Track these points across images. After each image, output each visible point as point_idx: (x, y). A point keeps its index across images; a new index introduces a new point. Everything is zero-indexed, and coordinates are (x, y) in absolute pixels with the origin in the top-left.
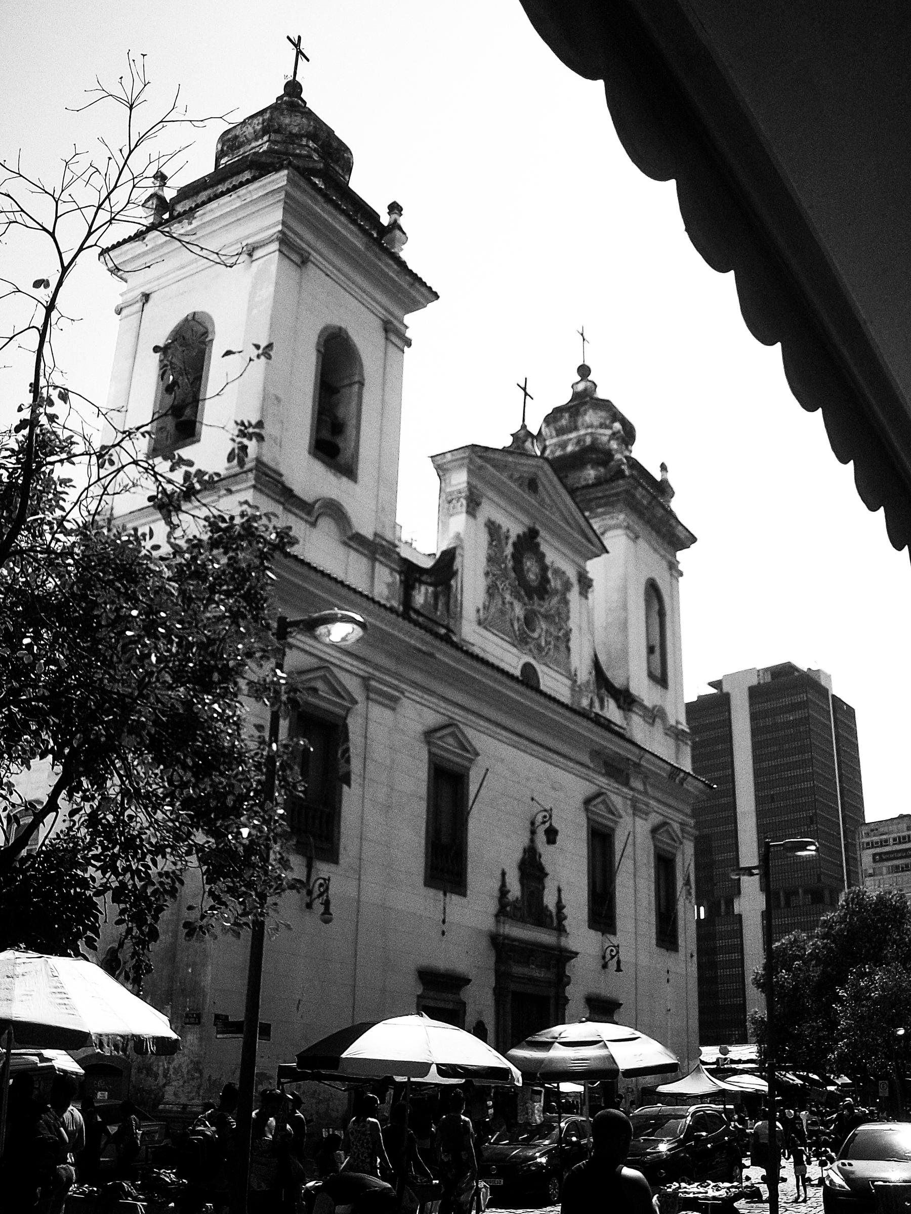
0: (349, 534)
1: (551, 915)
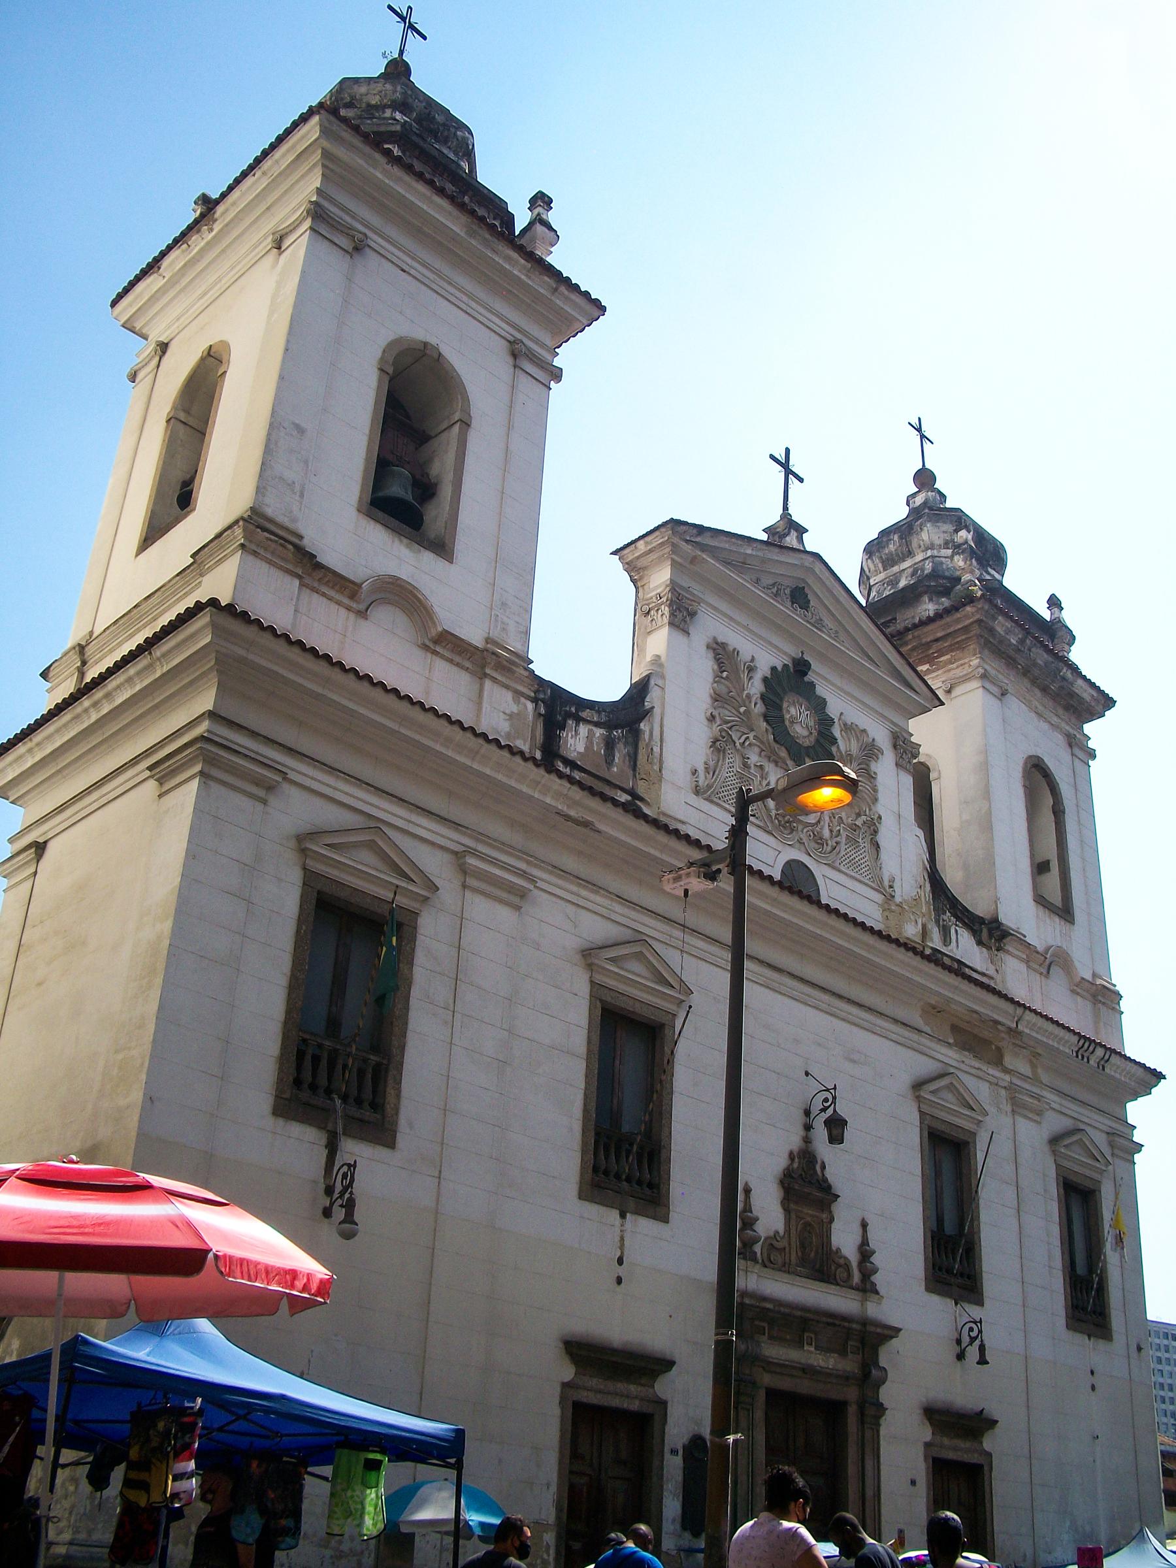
0: (433, 633)
1: (847, 1266)
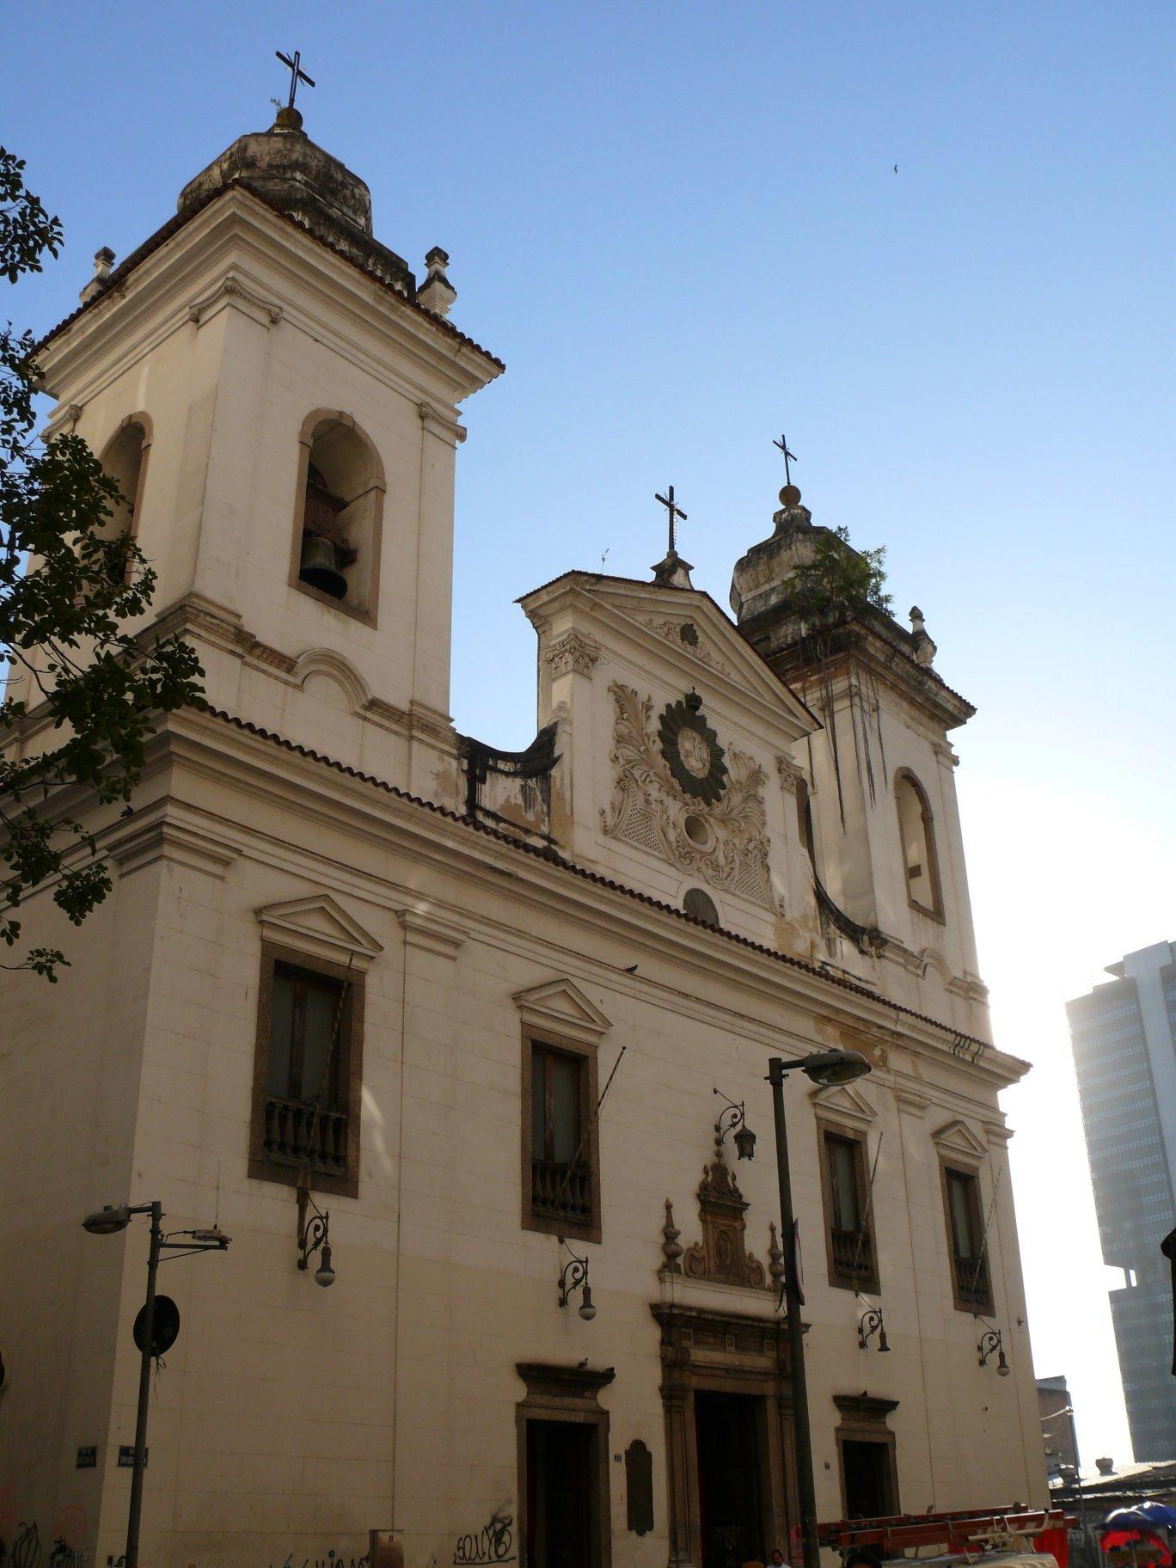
1: (759, 1267)
